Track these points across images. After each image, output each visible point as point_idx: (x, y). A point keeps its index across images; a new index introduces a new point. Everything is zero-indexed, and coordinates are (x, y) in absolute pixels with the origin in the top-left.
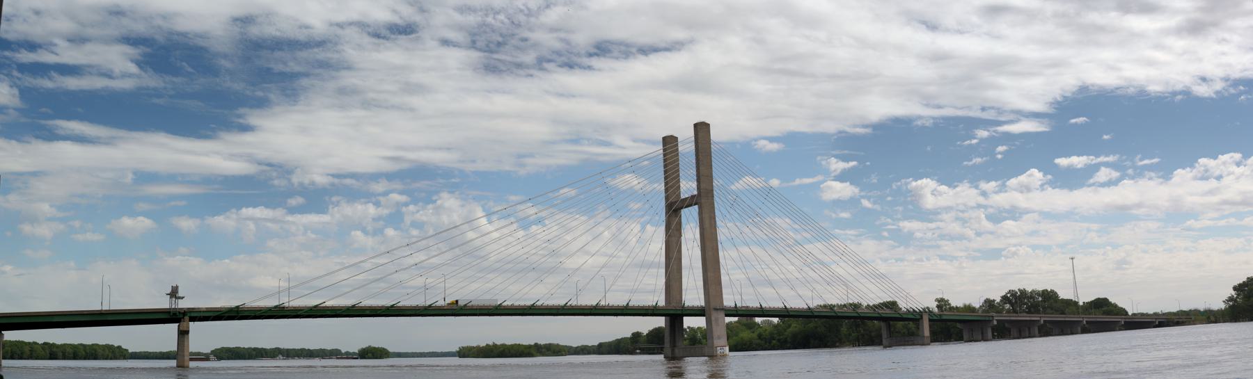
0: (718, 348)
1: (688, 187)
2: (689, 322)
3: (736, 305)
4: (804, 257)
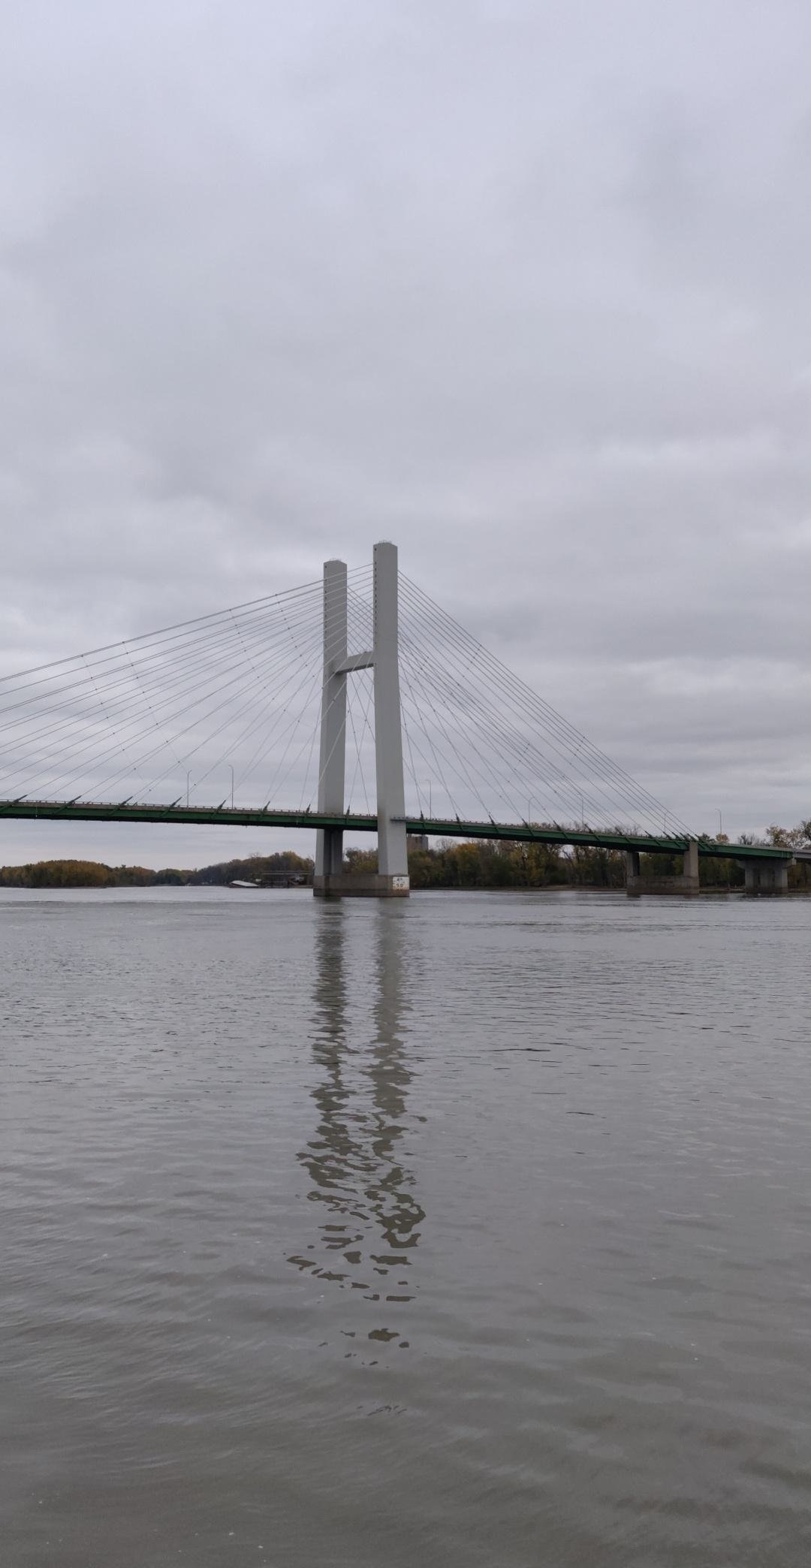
0: (395, 879)
1: (359, 640)
2: (355, 841)
3: (422, 815)
4: (575, 744)
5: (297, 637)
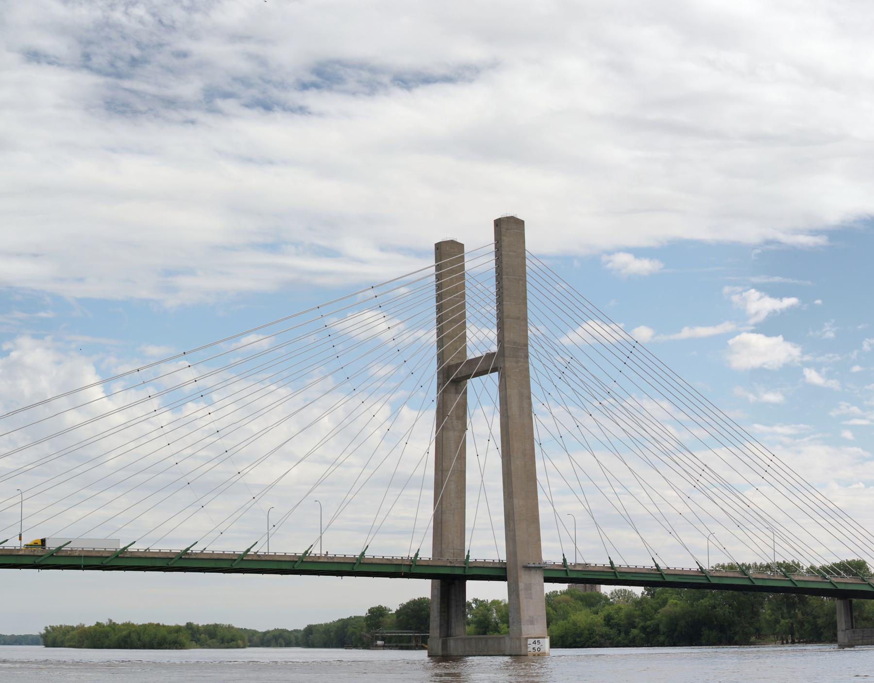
0: (530, 641)
3: (564, 560)
5: (607, 388)
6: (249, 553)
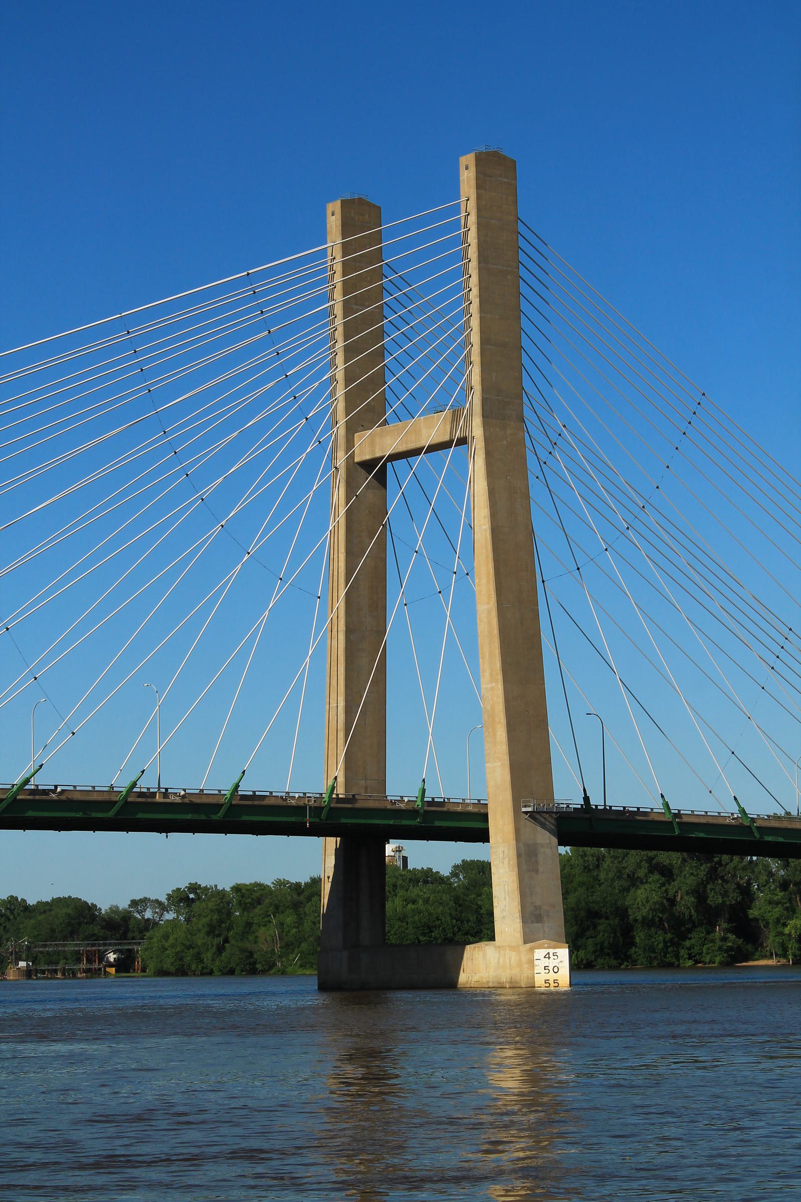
3: (586, 799)
6: (27, 787)
